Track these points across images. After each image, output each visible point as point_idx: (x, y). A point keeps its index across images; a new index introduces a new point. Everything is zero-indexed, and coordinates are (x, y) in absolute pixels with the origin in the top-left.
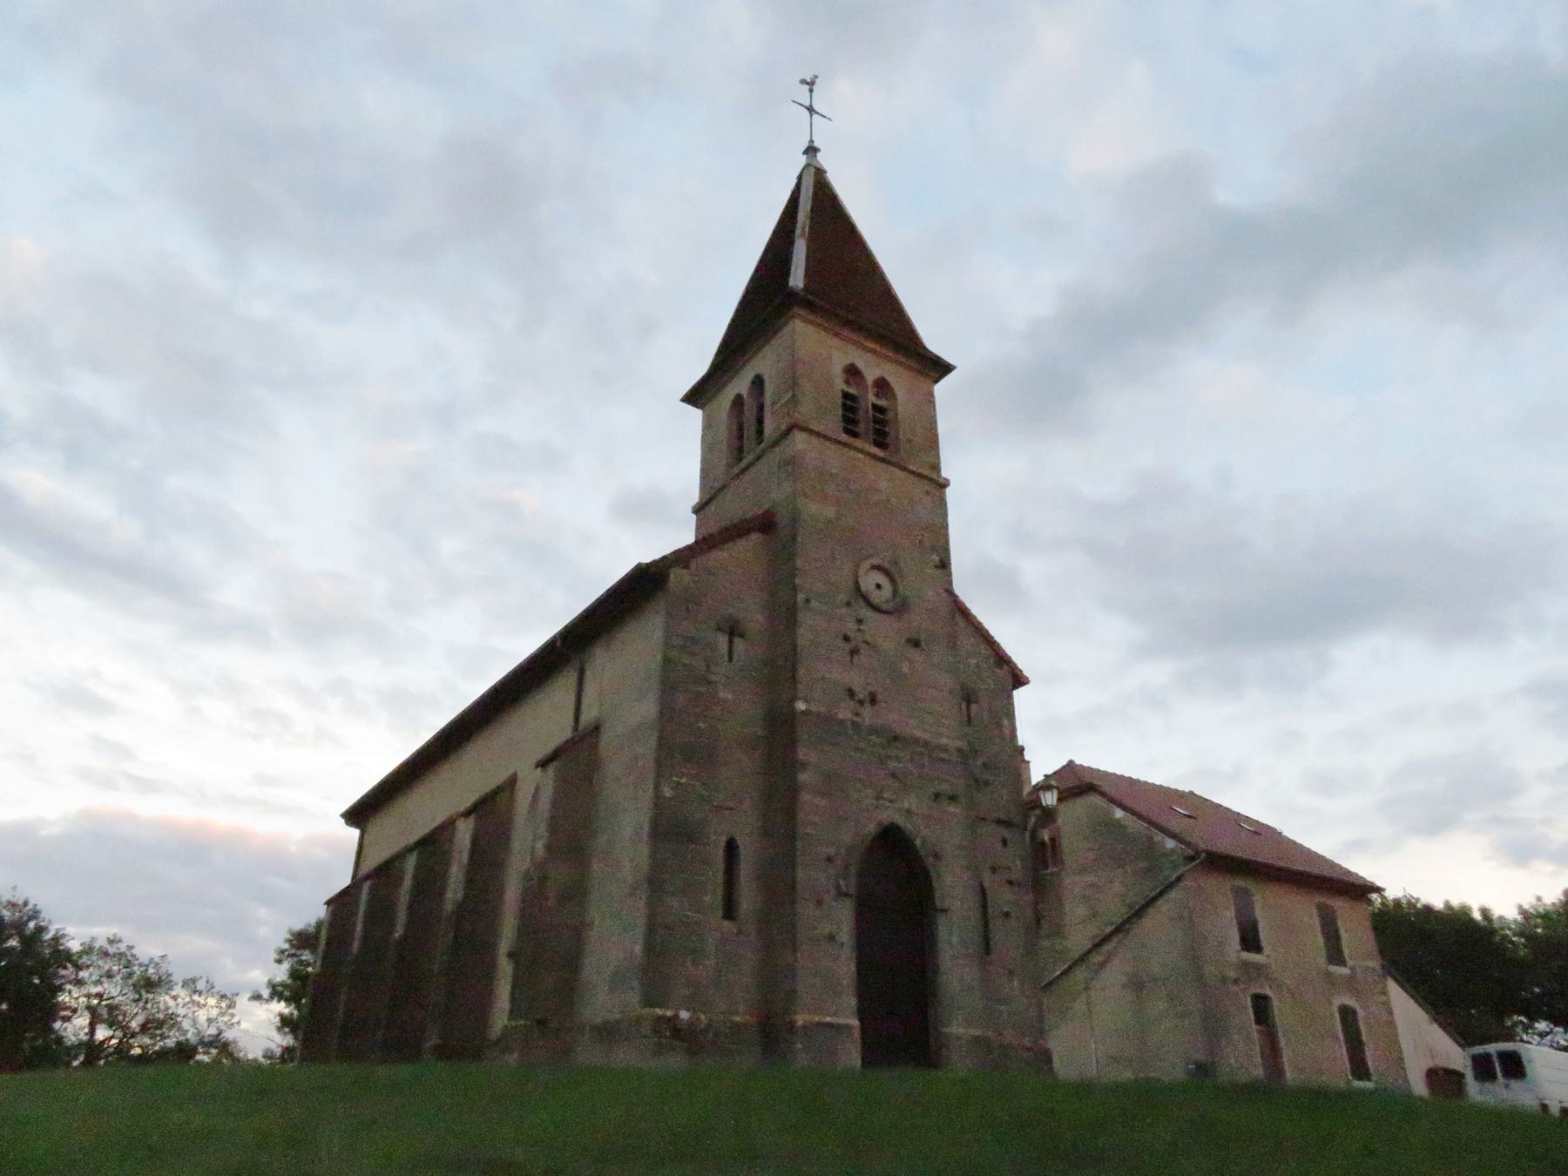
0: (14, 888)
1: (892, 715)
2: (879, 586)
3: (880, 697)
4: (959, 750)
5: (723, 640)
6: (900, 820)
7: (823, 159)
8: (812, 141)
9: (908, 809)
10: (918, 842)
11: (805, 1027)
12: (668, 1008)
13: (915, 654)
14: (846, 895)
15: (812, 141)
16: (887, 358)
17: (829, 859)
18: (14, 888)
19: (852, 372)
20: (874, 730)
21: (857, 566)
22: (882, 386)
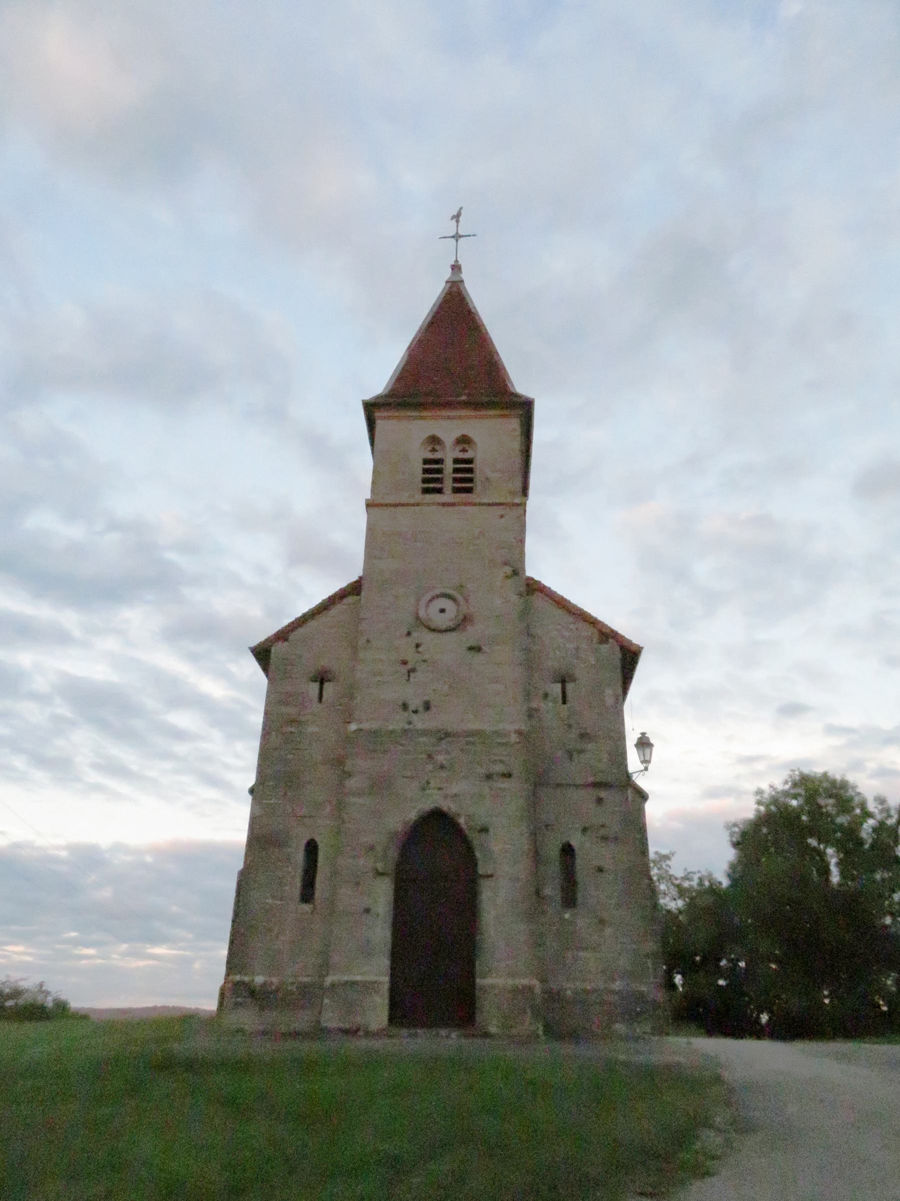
0: (686, 869)
1: (447, 718)
2: (442, 611)
3: (432, 703)
4: (519, 733)
5: (314, 687)
6: (448, 806)
7: (464, 276)
8: (457, 261)
9: (462, 795)
10: (462, 821)
11: (333, 985)
12: (246, 974)
13: (479, 658)
14: (382, 874)
15: (457, 261)
16: (470, 417)
17: (372, 848)
18: (686, 869)
19: (434, 441)
20: (425, 733)
21: (418, 600)
22: (464, 441)
